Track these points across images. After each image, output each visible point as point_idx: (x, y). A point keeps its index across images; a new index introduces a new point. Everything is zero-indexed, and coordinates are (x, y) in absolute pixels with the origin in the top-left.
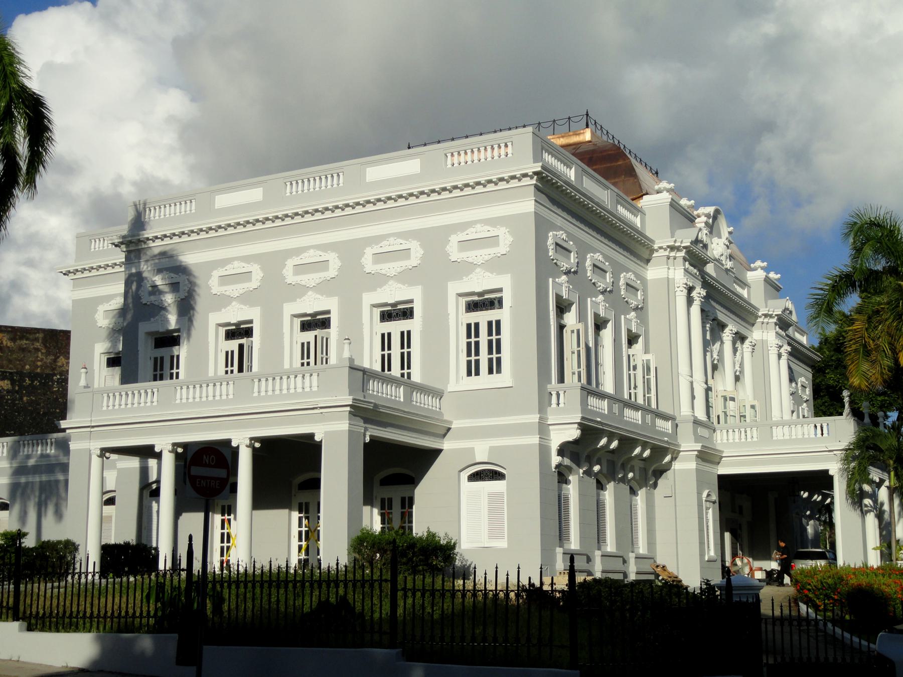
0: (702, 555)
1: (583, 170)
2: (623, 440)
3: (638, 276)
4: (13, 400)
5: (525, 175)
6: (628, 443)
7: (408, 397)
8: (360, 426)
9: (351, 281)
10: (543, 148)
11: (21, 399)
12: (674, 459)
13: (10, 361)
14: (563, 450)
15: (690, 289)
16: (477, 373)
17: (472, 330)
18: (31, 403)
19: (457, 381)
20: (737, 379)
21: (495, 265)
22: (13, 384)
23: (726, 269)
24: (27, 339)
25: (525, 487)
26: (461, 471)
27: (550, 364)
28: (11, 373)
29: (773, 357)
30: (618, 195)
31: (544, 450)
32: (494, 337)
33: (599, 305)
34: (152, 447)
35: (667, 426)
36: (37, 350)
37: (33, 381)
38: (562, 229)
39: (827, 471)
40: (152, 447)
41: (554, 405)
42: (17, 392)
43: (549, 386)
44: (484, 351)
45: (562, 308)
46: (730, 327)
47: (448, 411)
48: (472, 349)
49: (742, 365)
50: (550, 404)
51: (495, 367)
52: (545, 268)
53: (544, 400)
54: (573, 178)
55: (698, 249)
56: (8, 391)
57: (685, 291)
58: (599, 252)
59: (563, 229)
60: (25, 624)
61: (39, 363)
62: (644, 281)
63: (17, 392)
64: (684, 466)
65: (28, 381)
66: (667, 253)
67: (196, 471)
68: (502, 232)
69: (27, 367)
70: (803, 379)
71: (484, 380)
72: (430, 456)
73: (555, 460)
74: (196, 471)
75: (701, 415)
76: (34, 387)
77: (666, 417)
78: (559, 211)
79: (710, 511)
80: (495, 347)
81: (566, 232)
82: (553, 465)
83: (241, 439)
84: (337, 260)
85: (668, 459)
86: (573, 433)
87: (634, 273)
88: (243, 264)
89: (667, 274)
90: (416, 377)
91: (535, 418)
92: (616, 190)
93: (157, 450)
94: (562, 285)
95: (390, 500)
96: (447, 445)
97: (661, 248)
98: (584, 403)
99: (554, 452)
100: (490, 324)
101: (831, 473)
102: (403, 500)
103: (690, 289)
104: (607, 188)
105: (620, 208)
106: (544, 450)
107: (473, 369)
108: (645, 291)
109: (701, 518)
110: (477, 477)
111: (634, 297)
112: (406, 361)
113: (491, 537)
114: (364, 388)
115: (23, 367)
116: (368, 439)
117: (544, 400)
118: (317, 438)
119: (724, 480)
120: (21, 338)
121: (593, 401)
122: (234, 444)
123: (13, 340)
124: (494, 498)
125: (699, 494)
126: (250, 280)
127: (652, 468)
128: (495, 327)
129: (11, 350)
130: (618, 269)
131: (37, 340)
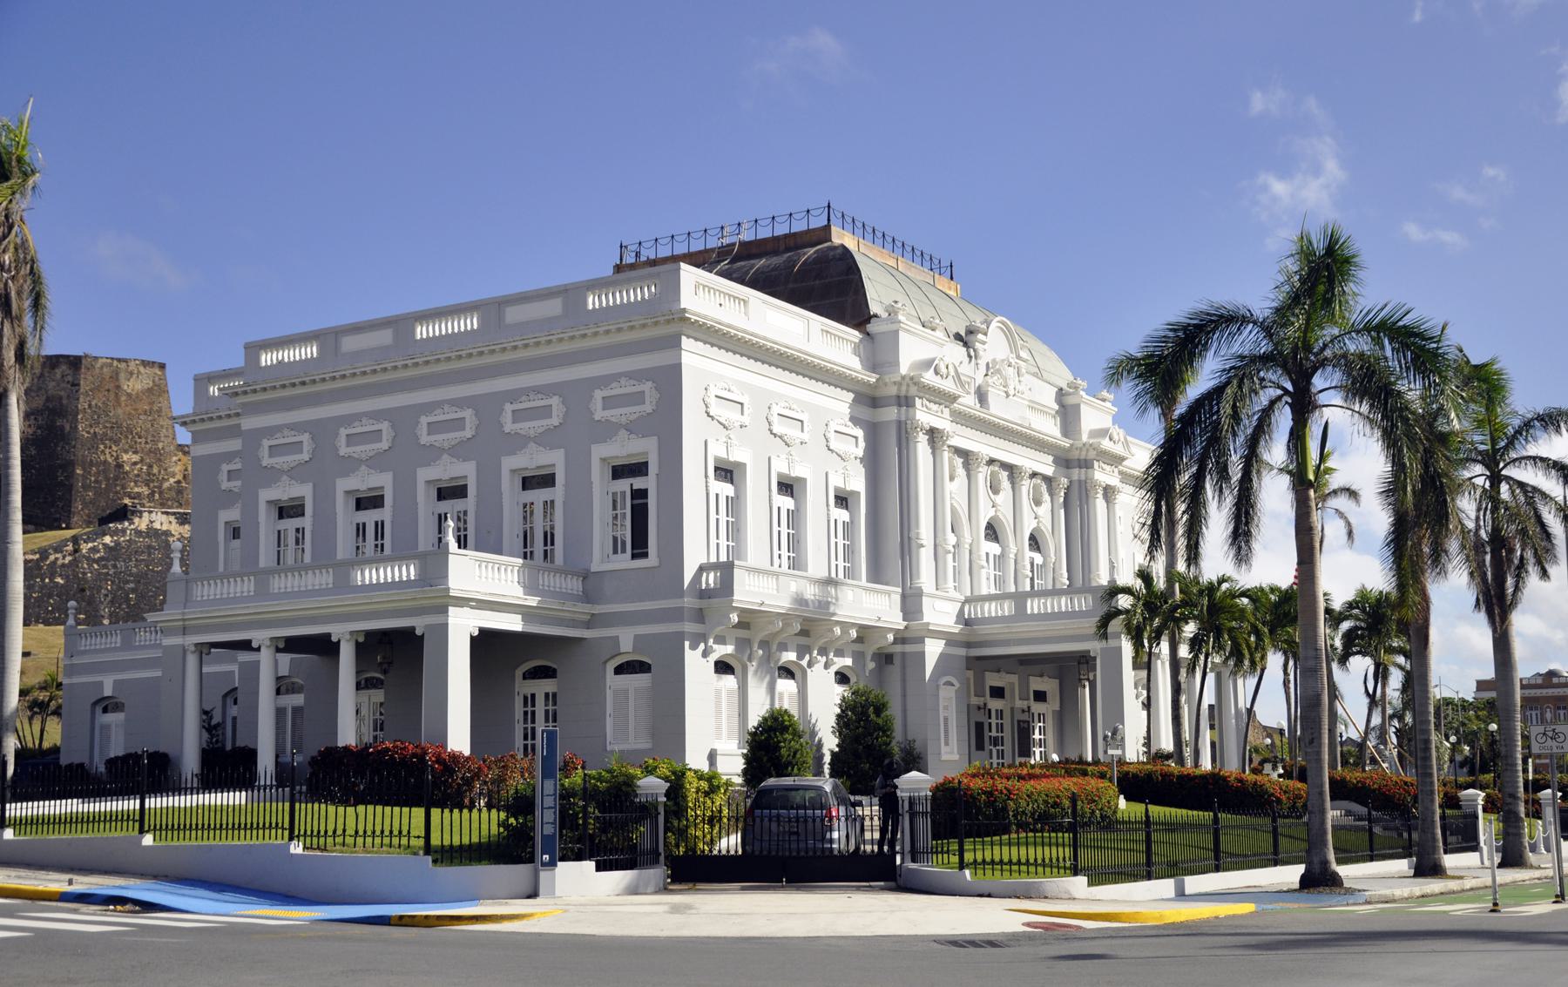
34: (249, 642)
40: (249, 642)
93: (254, 645)
95: (533, 696)
118: (418, 632)
122: (334, 639)
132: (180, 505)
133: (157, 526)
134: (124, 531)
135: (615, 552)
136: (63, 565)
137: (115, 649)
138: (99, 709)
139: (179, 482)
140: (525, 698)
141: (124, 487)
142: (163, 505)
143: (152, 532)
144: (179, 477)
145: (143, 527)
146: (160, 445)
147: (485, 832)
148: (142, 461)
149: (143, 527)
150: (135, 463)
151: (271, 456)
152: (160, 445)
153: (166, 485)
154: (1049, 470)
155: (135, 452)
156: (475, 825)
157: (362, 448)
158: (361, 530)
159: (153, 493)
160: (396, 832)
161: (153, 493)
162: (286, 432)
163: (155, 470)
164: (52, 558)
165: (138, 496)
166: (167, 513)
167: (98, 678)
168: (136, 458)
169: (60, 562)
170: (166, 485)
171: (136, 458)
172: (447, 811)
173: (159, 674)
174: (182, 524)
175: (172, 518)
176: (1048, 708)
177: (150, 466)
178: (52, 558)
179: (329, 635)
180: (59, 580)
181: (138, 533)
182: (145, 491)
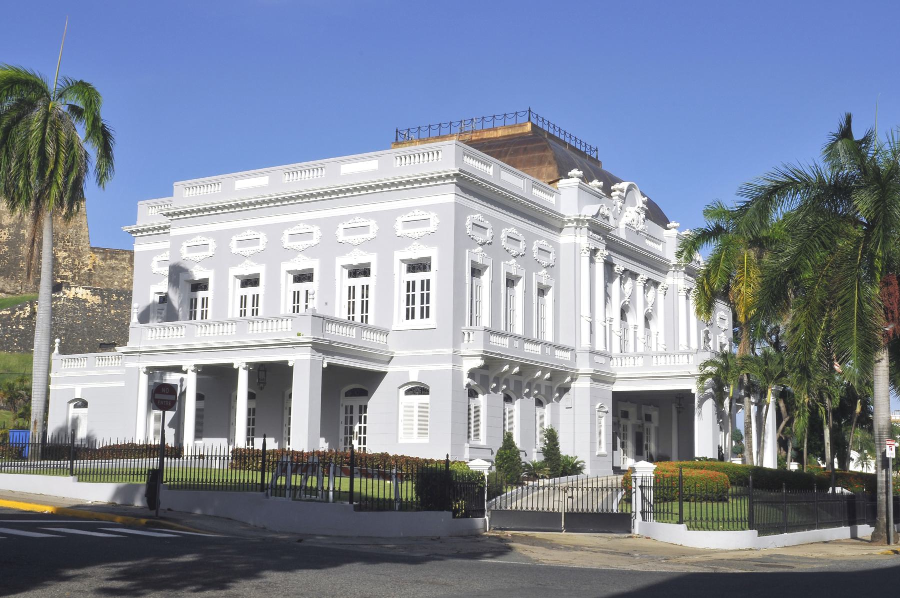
0: (592, 451)
1: (501, 166)
2: (523, 366)
3: (549, 242)
4: (103, 313)
5: (448, 176)
6: (527, 369)
7: (359, 335)
8: (319, 356)
9: (329, 247)
10: (464, 154)
11: (109, 311)
12: (572, 380)
13: (101, 278)
14: (472, 374)
15: (594, 252)
16: (413, 318)
17: (410, 286)
18: (117, 315)
19: (399, 322)
20: (647, 318)
21: (428, 239)
22: (102, 299)
23: (638, 232)
24: (117, 259)
25: (442, 399)
26: (400, 388)
27: (463, 310)
28: (101, 290)
29: (682, 298)
30: (534, 182)
31: (456, 375)
32: (425, 292)
33: (512, 266)
34: (181, 367)
35: (567, 355)
36: (124, 268)
37: (119, 297)
38: (479, 212)
39: (690, 390)
40: (181, 367)
41: (466, 342)
42: (106, 306)
43: (463, 328)
44: (417, 303)
45: (476, 272)
46: (641, 276)
47: (392, 345)
48: (410, 300)
49: (654, 305)
50: (463, 341)
51: (425, 313)
52: (462, 241)
53: (458, 337)
54: (491, 174)
55: (600, 220)
56: (99, 305)
57: (588, 254)
58: (514, 225)
59: (479, 211)
60: (76, 477)
61: (126, 280)
62: (556, 246)
63: (106, 306)
64: (581, 386)
65: (115, 297)
66: (575, 224)
67: (157, 396)
68: (432, 215)
69: (116, 283)
70: (722, 313)
71: (418, 322)
72: (378, 377)
73: (466, 380)
74: (157, 396)
75: (599, 346)
76: (120, 302)
77: (566, 349)
78: (476, 200)
79: (603, 420)
80: (426, 299)
81: (482, 214)
82: (465, 385)
83: (240, 361)
84: (319, 232)
85: (568, 379)
86: (479, 362)
87: (546, 239)
88: (253, 232)
89: (572, 241)
90: (371, 322)
91: (450, 350)
92: (532, 178)
93: (184, 369)
94: (478, 255)
95: (352, 407)
96: (390, 369)
97: (569, 221)
98: (487, 341)
99: (465, 375)
100: (423, 282)
101: (693, 392)
102: (361, 407)
103: (594, 252)
104: (524, 177)
105: (535, 191)
106: (456, 375)
107: (410, 314)
108: (557, 253)
109: (593, 423)
110: (409, 392)
111: (546, 259)
112: (365, 307)
113: (420, 435)
114: (323, 330)
115: (112, 283)
116: (325, 365)
117: (458, 337)
118: (290, 364)
119: (618, 397)
120: (111, 259)
121: (494, 339)
122: (235, 367)
123: (104, 259)
124: (422, 407)
125: (592, 405)
126: (258, 244)
127: (558, 385)
128: (425, 285)
129: (102, 269)
130: (530, 238)
131: (124, 260)
132: (90, 284)
133: (79, 296)
134: (60, 298)
135: (408, 318)
136: (24, 318)
137: (83, 369)
138: (72, 405)
139: (90, 270)
140: (346, 407)
141: (58, 272)
142: (80, 284)
143: (76, 300)
144: (90, 267)
145: (71, 297)
146: (80, 247)
147: (585, 507)
148: (69, 256)
149: (71, 297)
150: (65, 258)
151: (239, 246)
152: (80, 247)
153: (83, 271)
154: (617, 280)
155: (65, 251)
156: (704, 511)
157: (247, 249)
158: (243, 300)
159: (74, 276)
160: (704, 518)
161: (74, 276)
162: (357, 219)
163: (77, 262)
164: (18, 313)
165: (66, 278)
166: (86, 289)
167: (70, 386)
168: (65, 254)
169: (22, 316)
170: (83, 271)
171: (65, 254)
172: (151, 467)
173: (123, 384)
174: (94, 295)
175: (88, 292)
176: (655, 423)
177: (74, 260)
178: (18, 313)
179: (232, 364)
180: (21, 327)
181: (68, 300)
182: (69, 274)
